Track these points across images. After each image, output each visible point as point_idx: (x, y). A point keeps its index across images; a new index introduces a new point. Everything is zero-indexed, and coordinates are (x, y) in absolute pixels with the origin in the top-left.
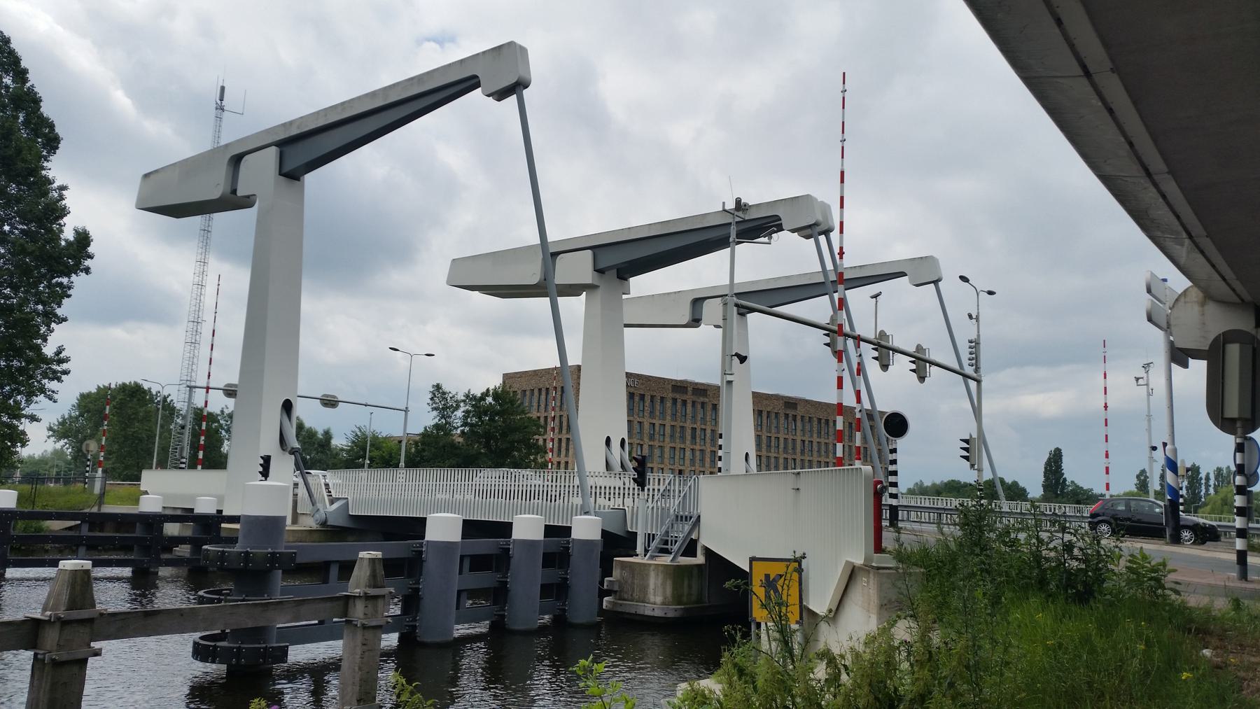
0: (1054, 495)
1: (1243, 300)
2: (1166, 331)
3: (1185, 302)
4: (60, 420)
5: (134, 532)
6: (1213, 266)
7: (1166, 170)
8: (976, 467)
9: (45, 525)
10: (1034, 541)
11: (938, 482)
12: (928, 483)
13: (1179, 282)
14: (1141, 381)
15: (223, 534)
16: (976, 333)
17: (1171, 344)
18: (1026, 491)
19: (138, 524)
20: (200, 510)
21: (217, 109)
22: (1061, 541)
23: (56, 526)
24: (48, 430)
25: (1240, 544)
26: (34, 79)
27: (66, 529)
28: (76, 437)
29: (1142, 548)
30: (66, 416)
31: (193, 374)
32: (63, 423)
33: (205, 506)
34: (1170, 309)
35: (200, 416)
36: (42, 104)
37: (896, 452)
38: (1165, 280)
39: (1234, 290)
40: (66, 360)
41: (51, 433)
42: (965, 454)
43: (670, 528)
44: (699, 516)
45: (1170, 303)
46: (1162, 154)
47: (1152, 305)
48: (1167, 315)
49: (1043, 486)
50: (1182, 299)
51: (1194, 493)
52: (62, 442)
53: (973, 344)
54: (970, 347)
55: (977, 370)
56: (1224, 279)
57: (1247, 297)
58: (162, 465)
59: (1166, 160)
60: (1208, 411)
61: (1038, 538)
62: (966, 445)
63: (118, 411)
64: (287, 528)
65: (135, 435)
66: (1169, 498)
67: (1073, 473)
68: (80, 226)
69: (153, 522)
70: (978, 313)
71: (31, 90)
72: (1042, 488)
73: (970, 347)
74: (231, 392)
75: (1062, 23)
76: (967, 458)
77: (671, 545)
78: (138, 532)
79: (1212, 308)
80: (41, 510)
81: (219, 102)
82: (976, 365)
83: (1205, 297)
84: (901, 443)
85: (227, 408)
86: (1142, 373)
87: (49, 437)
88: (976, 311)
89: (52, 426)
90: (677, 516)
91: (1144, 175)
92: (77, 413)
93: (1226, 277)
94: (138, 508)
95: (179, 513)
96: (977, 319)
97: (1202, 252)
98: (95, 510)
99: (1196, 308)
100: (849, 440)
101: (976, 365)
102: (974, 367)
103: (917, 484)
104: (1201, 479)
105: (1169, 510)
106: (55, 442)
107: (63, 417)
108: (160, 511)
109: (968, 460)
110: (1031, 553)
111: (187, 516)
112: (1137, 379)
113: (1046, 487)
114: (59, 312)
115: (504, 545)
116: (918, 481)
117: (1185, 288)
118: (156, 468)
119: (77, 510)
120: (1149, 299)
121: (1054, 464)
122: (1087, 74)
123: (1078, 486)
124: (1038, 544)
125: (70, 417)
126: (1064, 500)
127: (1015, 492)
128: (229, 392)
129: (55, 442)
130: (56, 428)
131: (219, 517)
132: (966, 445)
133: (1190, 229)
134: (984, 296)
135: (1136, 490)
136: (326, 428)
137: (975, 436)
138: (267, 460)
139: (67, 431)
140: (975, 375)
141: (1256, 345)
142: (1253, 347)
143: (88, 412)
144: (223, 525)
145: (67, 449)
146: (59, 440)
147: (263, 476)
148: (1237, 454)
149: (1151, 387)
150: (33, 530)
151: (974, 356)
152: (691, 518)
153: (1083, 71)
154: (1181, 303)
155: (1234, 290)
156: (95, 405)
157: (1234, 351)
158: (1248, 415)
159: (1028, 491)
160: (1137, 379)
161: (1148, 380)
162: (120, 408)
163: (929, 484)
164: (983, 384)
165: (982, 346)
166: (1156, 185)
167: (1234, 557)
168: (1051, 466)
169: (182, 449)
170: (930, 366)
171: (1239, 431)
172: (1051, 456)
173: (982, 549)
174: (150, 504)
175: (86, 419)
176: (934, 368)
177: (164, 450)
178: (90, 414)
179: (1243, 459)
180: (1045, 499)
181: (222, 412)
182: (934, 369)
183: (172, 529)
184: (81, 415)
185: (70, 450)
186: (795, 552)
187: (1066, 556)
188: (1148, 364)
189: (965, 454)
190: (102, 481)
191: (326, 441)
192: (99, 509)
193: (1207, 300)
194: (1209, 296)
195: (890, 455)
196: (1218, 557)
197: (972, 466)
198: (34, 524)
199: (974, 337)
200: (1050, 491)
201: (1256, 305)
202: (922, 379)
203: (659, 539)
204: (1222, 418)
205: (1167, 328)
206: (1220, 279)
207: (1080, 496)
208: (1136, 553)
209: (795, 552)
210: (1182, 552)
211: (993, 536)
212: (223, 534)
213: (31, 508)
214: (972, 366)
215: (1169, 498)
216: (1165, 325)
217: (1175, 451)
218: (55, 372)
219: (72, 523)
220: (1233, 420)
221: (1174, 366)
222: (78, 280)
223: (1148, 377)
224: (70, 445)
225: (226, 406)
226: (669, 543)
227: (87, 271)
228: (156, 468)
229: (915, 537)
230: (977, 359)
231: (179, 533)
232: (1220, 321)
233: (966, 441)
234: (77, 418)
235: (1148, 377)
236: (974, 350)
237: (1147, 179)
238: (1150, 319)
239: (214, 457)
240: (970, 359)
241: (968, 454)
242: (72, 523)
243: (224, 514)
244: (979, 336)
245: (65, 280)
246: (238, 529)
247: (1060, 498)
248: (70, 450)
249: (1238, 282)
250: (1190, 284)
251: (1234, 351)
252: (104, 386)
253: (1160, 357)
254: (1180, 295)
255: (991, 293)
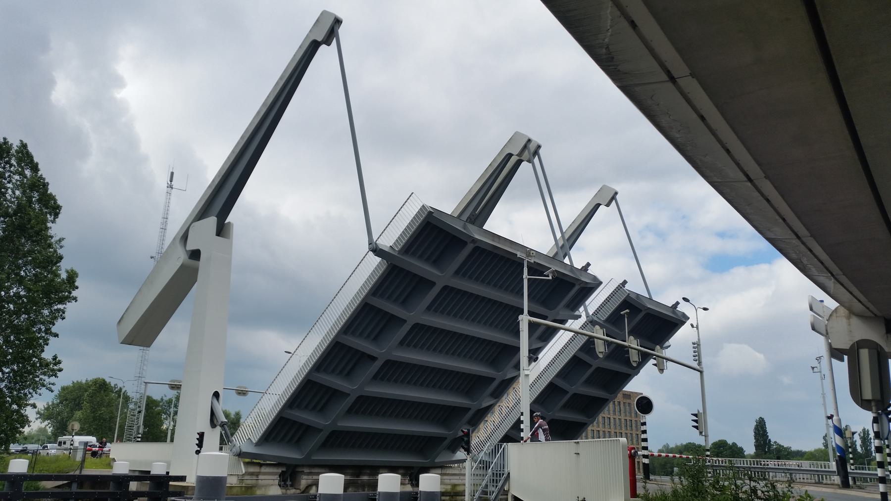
0: (763, 453)
1: (875, 315)
2: (826, 336)
3: (837, 317)
4: (46, 406)
5: (108, 489)
6: (851, 293)
7: (809, 235)
8: (703, 434)
9: (42, 484)
10: (733, 487)
11: (679, 444)
12: (672, 445)
13: (831, 304)
14: (815, 370)
15: (171, 489)
16: (697, 337)
17: (830, 345)
18: (743, 450)
19: (111, 483)
20: (154, 472)
21: (168, 187)
22: (749, 486)
23: (49, 485)
24: (37, 414)
25: (882, 488)
26: (43, 172)
27: (56, 487)
28: (56, 418)
29: (806, 491)
30: (50, 404)
31: (144, 373)
32: (47, 409)
33: (158, 469)
34: (827, 320)
35: (151, 403)
36: (49, 187)
37: (646, 425)
38: (822, 301)
39: (868, 308)
40: (60, 362)
41: (38, 416)
42: (695, 424)
43: (489, 482)
44: (509, 473)
45: (826, 317)
46: (805, 225)
47: (814, 319)
48: (826, 325)
49: (755, 445)
50: (835, 315)
51: (866, 449)
52: (46, 422)
53: (696, 345)
54: (694, 348)
55: (700, 364)
56: (860, 301)
57: (878, 313)
58: (120, 439)
59: (808, 229)
60: (853, 398)
61: (736, 485)
62: (695, 418)
63: (90, 399)
64: (227, 485)
65: (101, 416)
66: (838, 454)
67: (775, 435)
68: (69, 268)
69: (122, 481)
70: (698, 323)
71: (41, 177)
72: (754, 447)
73: (694, 348)
74: (174, 386)
75: (730, 152)
76: (696, 427)
77: (490, 495)
78: (111, 489)
79: (855, 321)
80: (39, 474)
81: (169, 183)
82: (699, 361)
83: (850, 313)
84: (648, 418)
85: (165, 396)
86: (815, 364)
87: (37, 419)
88: (696, 322)
89: (40, 410)
90: (493, 474)
91: (796, 237)
92: (58, 401)
93: (861, 300)
94: (112, 471)
95: (137, 474)
96: (697, 327)
97: (842, 284)
98: (77, 473)
99: (845, 321)
100: (613, 414)
101: (699, 361)
102: (697, 362)
103: (665, 446)
104: (871, 439)
105: (839, 463)
106: (41, 423)
107: (48, 404)
108: (127, 473)
109: (698, 429)
110: (731, 495)
111: (143, 476)
112: (813, 368)
113: (757, 446)
114: (54, 329)
115: (372, 496)
116: (665, 444)
117: (836, 307)
118: (117, 442)
119: (65, 473)
120: (812, 315)
121: (761, 429)
122: (750, 180)
123: (780, 445)
124: (736, 489)
125: (53, 404)
126: (772, 455)
127: (736, 451)
128: (173, 386)
129: (41, 423)
130: (42, 412)
131: (167, 478)
132: (695, 418)
133: (831, 270)
134: (701, 311)
135: (824, 448)
136: (237, 410)
137: (701, 411)
138: (201, 436)
139: (50, 414)
140: (698, 367)
141: (879, 350)
142: (878, 351)
143: (66, 400)
144: (171, 483)
145: (50, 427)
146: (44, 421)
147: (198, 447)
148: (874, 424)
149: (823, 373)
150: (33, 488)
151: (697, 354)
152: (503, 474)
153: (747, 178)
154: (834, 317)
155: (868, 308)
156: (71, 395)
157: (864, 354)
158: (878, 397)
159: (744, 450)
160: (813, 368)
161: (821, 369)
162: (92, 397)
163: (674, 446)
164: (705, 374)
165: (702, 347)
166: (803, 243)
167: (879, 497)
168: (758, 430)
169: (139, 427)
170: (666, 362)
171: (874, 408)
172: (758, 424)
173: (699, 493)
174: (121, 468)
175: (65, 405)
176: (669, 363)
177: (122, 428)
178: (67, 402)
179: (878, 428)
180: (757, 455)
181: (162, 399)
182: (669, 364)
183: (133, 486)
184: (61, 402)
185: (51, 428)
186: (578, 497)
187: (753, 497)
188: (819, 357)
189: (695, 424)
190: (83, 452)
191: (237, 420)
192: (81, 473)
193: (851, 315)
194: (852, 312)
195: (642, 427)
196: (876, 497)
197: (701, 433)
198: (33, 483)
199: (696, 340)
200: (760, 449)
201: (885, 319)
202: (661, 370)
203: (481, 491)
204: (861, 399)
205: (826, 335)
206: (857, 302)
207: (783, 453)
208: (803, 494)
209: (578, 497)
210: (851, 494)
211: (708, 484)
212: (171, 489)
213: (32, 472)
214: (696, 361)
215: (838, 454)
216: (824, 333)
217: (840, 420)
218: (53, 370)
219: (61, 483)
220: (869, 401)
221: (834, 360)
222: (70, 307)
223: (820, 366)
224: (51, 425)
225: (165, 395)
226: (489, 494)
227: (75, 299)
228: (117, 442)
229: (656, 486)
230: (699, 356)
231: (137, 489)
232: (862, 331)
233: (696, 415)
234: (58, 405)
235: (820, 366)
236: (696, 349)
237: (798, 240)
238: (813, 329)
239: (156, 432)
240: (694, 356)
241: (697, 425)
242: (61, 483)
243: (170, 475)
244: (699, 339)
245: (60, 306)
246: (194, 486)
247: (768, 454)
248: (51, 428)
249: (869, 303)
250: (838, 305)
251: (864, 354)
252: (77, 381)
253: (824, 351)
254: (834, 310)
255: (705, 309)
